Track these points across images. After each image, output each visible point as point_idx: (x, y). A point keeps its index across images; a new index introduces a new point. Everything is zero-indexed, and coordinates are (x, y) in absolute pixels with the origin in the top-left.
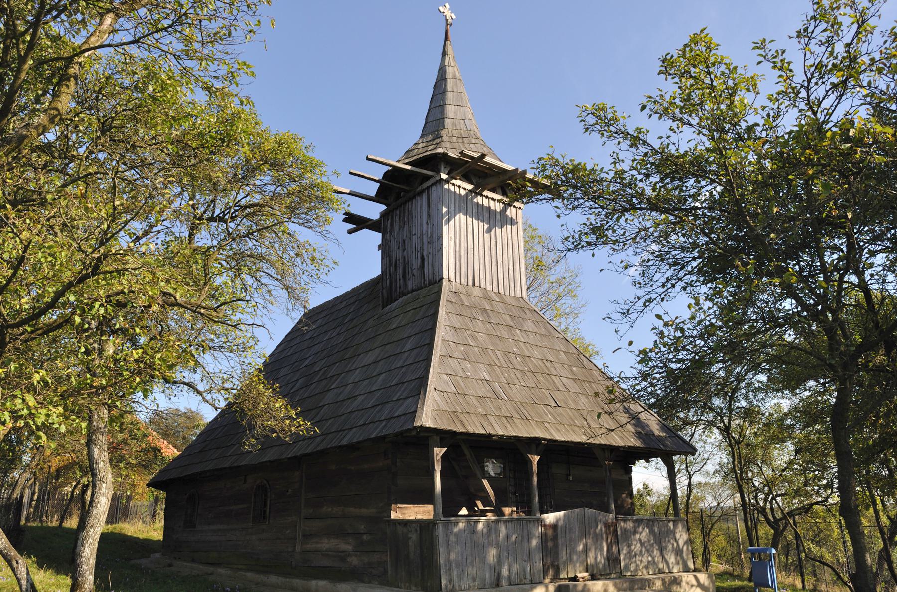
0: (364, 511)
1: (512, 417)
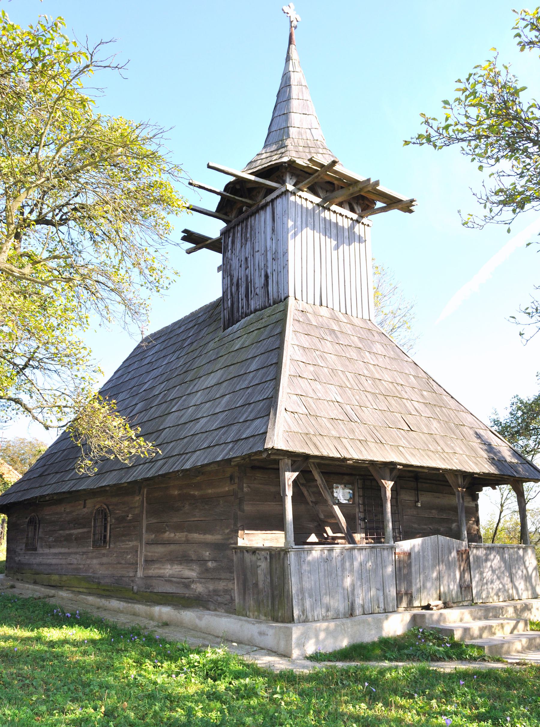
0: (209, 538)
1: (366, 441)
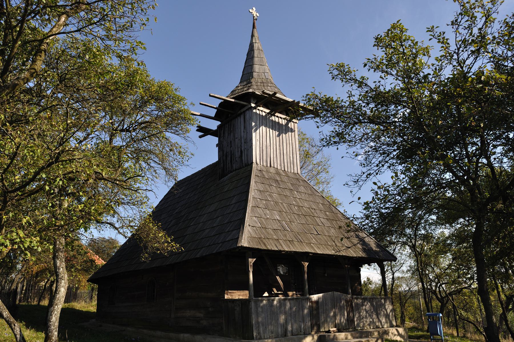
1: (293, 241)
